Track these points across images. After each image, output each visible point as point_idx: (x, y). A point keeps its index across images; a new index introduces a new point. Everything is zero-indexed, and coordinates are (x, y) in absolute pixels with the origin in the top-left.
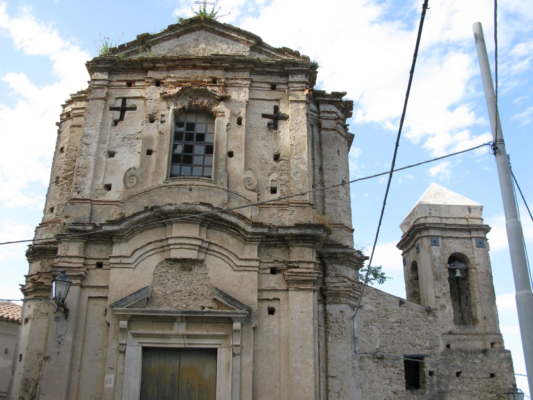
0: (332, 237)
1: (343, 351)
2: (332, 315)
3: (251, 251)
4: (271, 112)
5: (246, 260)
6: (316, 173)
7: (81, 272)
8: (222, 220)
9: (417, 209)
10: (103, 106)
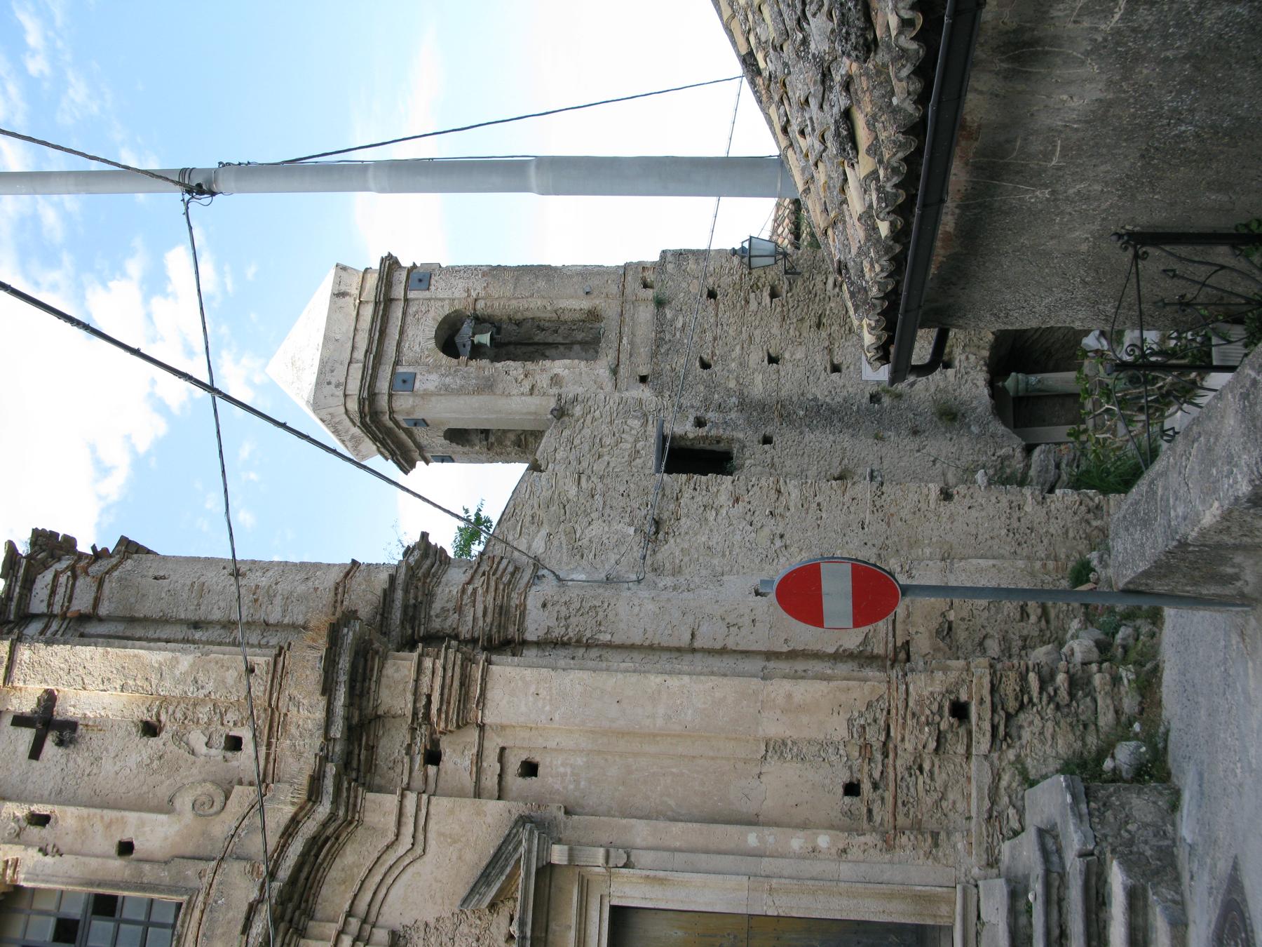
0: (365, 611)
1: (636, 609)
3: (380, 809)
5: (399, 824)
6: (204, 638)
8: (293, 880)
9: (324, 413)
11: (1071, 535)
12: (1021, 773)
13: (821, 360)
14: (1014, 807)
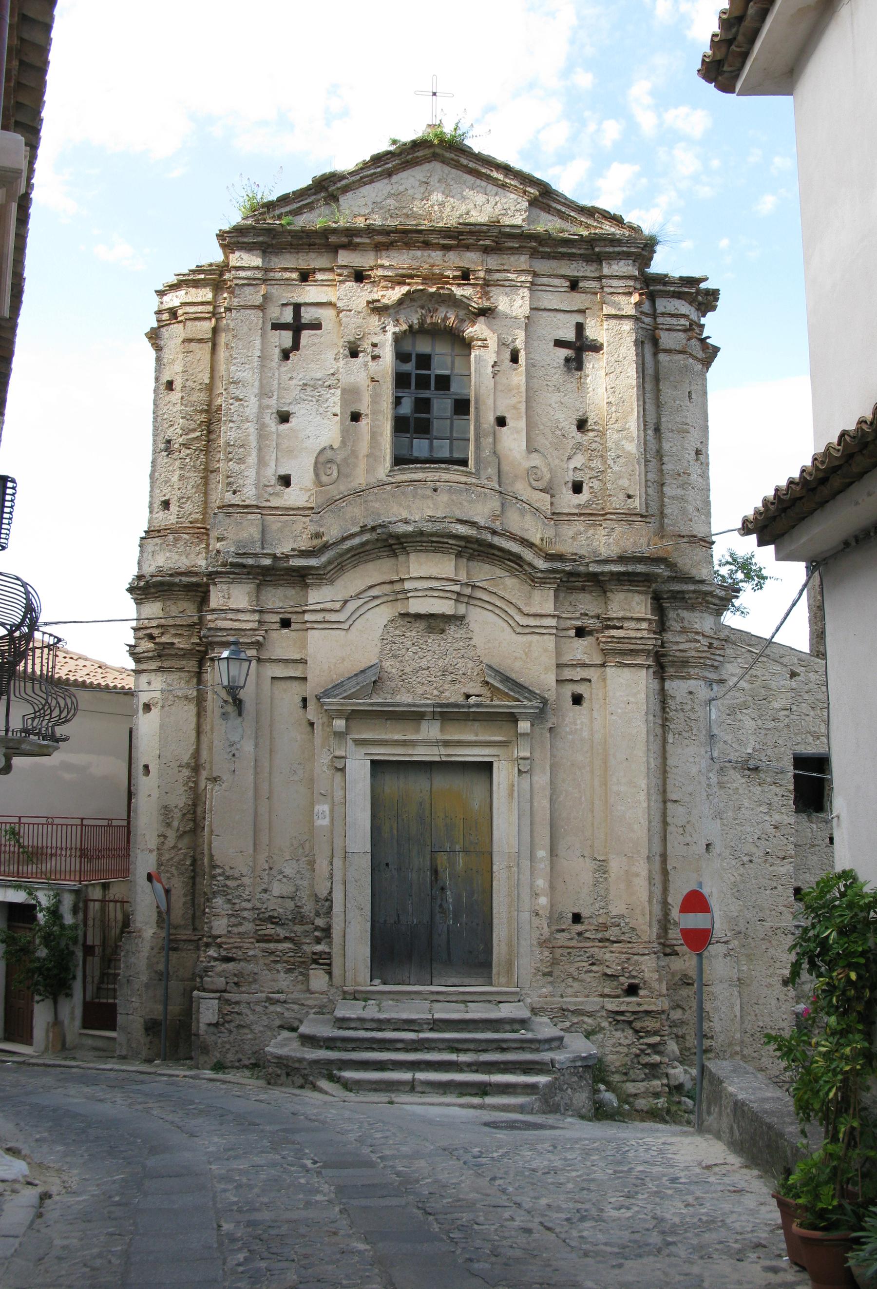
1: (692, 760)
3: (543, 601)
4: (570, 335)
5: (535, 615)
7: (258, 638)
8: (492, 546)
10: (261, 321)
12: (593, 1030)
14: (571, 1026)
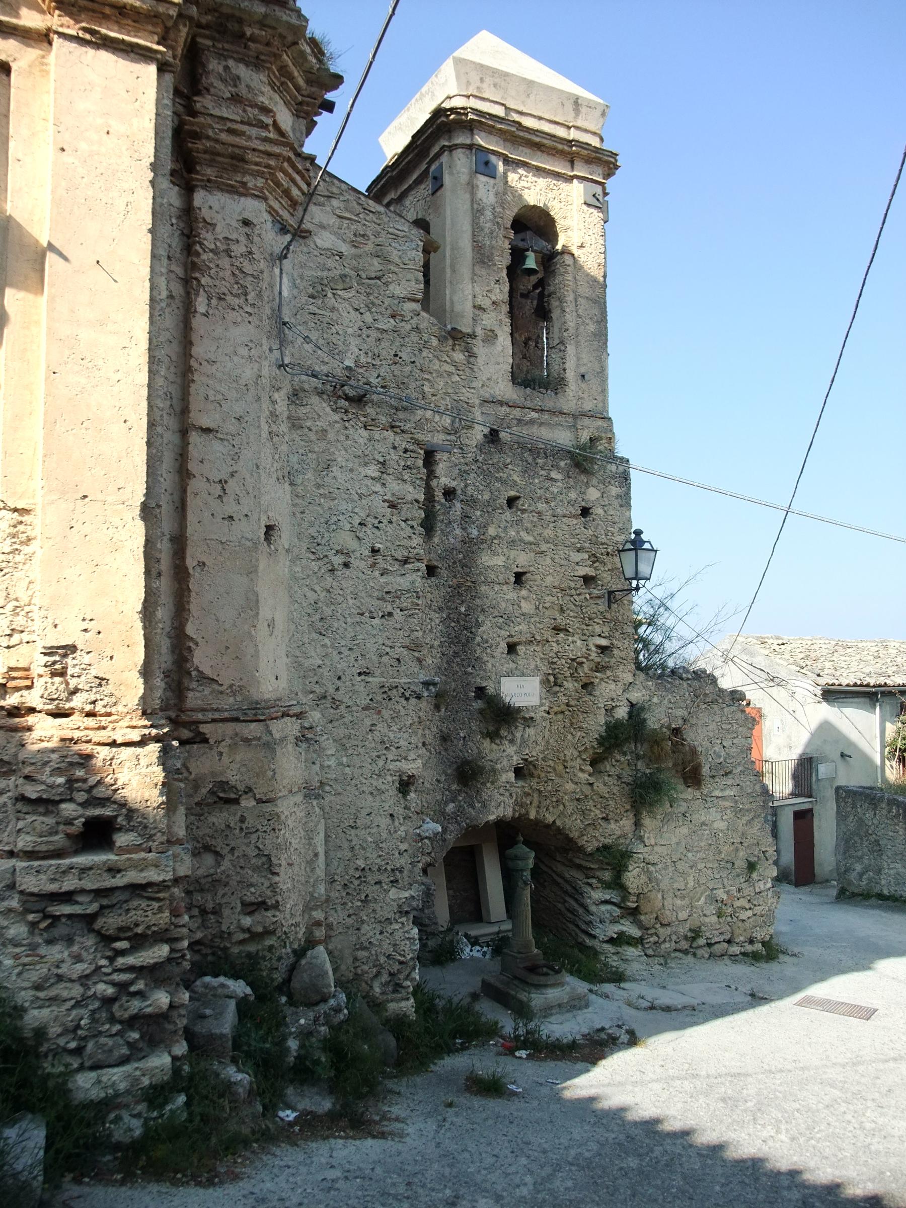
1: (244, 351)
2: (214, 225)
11: (362, 954)
13: (521, 630)
